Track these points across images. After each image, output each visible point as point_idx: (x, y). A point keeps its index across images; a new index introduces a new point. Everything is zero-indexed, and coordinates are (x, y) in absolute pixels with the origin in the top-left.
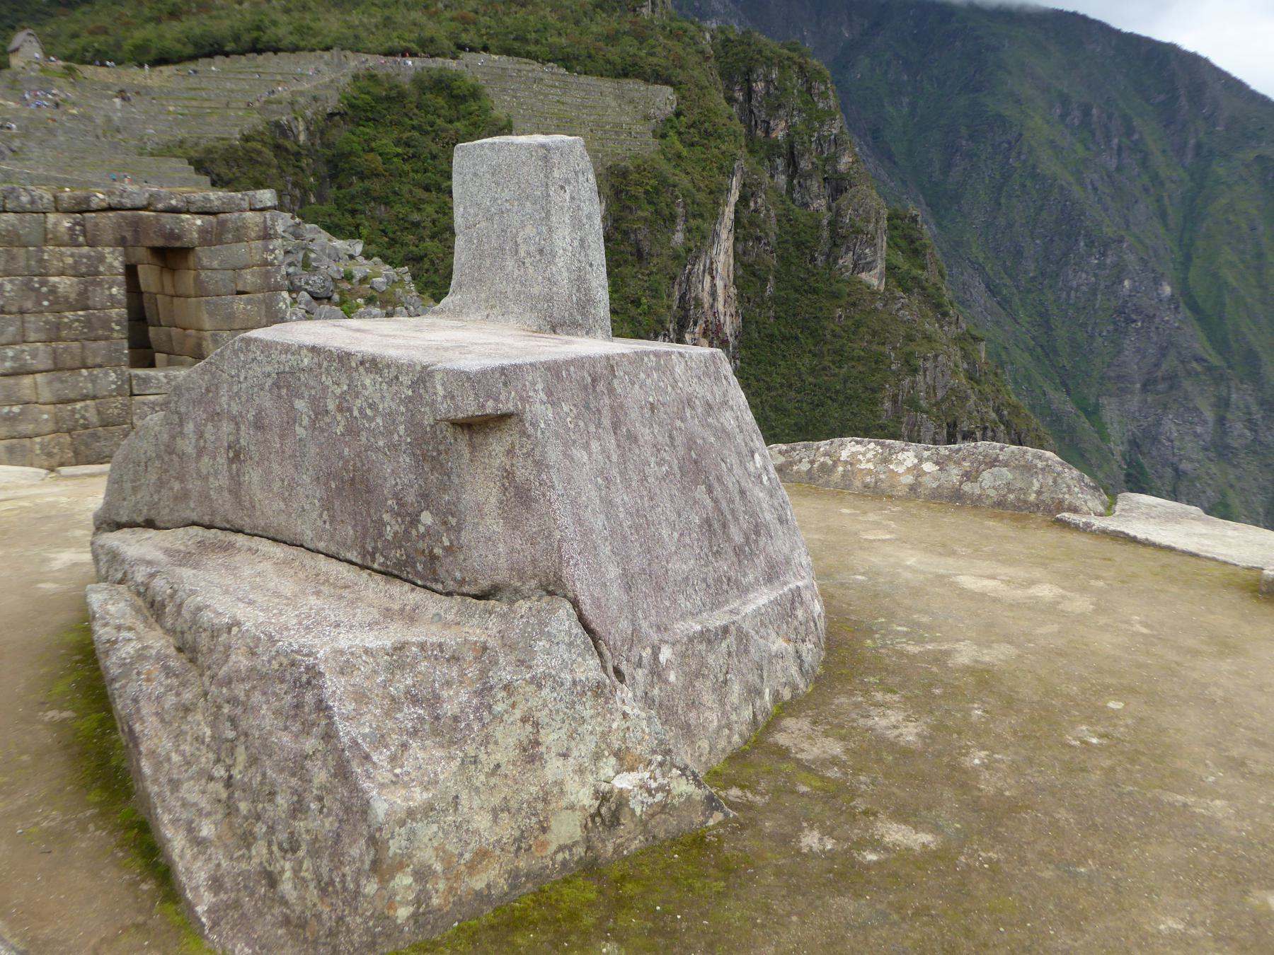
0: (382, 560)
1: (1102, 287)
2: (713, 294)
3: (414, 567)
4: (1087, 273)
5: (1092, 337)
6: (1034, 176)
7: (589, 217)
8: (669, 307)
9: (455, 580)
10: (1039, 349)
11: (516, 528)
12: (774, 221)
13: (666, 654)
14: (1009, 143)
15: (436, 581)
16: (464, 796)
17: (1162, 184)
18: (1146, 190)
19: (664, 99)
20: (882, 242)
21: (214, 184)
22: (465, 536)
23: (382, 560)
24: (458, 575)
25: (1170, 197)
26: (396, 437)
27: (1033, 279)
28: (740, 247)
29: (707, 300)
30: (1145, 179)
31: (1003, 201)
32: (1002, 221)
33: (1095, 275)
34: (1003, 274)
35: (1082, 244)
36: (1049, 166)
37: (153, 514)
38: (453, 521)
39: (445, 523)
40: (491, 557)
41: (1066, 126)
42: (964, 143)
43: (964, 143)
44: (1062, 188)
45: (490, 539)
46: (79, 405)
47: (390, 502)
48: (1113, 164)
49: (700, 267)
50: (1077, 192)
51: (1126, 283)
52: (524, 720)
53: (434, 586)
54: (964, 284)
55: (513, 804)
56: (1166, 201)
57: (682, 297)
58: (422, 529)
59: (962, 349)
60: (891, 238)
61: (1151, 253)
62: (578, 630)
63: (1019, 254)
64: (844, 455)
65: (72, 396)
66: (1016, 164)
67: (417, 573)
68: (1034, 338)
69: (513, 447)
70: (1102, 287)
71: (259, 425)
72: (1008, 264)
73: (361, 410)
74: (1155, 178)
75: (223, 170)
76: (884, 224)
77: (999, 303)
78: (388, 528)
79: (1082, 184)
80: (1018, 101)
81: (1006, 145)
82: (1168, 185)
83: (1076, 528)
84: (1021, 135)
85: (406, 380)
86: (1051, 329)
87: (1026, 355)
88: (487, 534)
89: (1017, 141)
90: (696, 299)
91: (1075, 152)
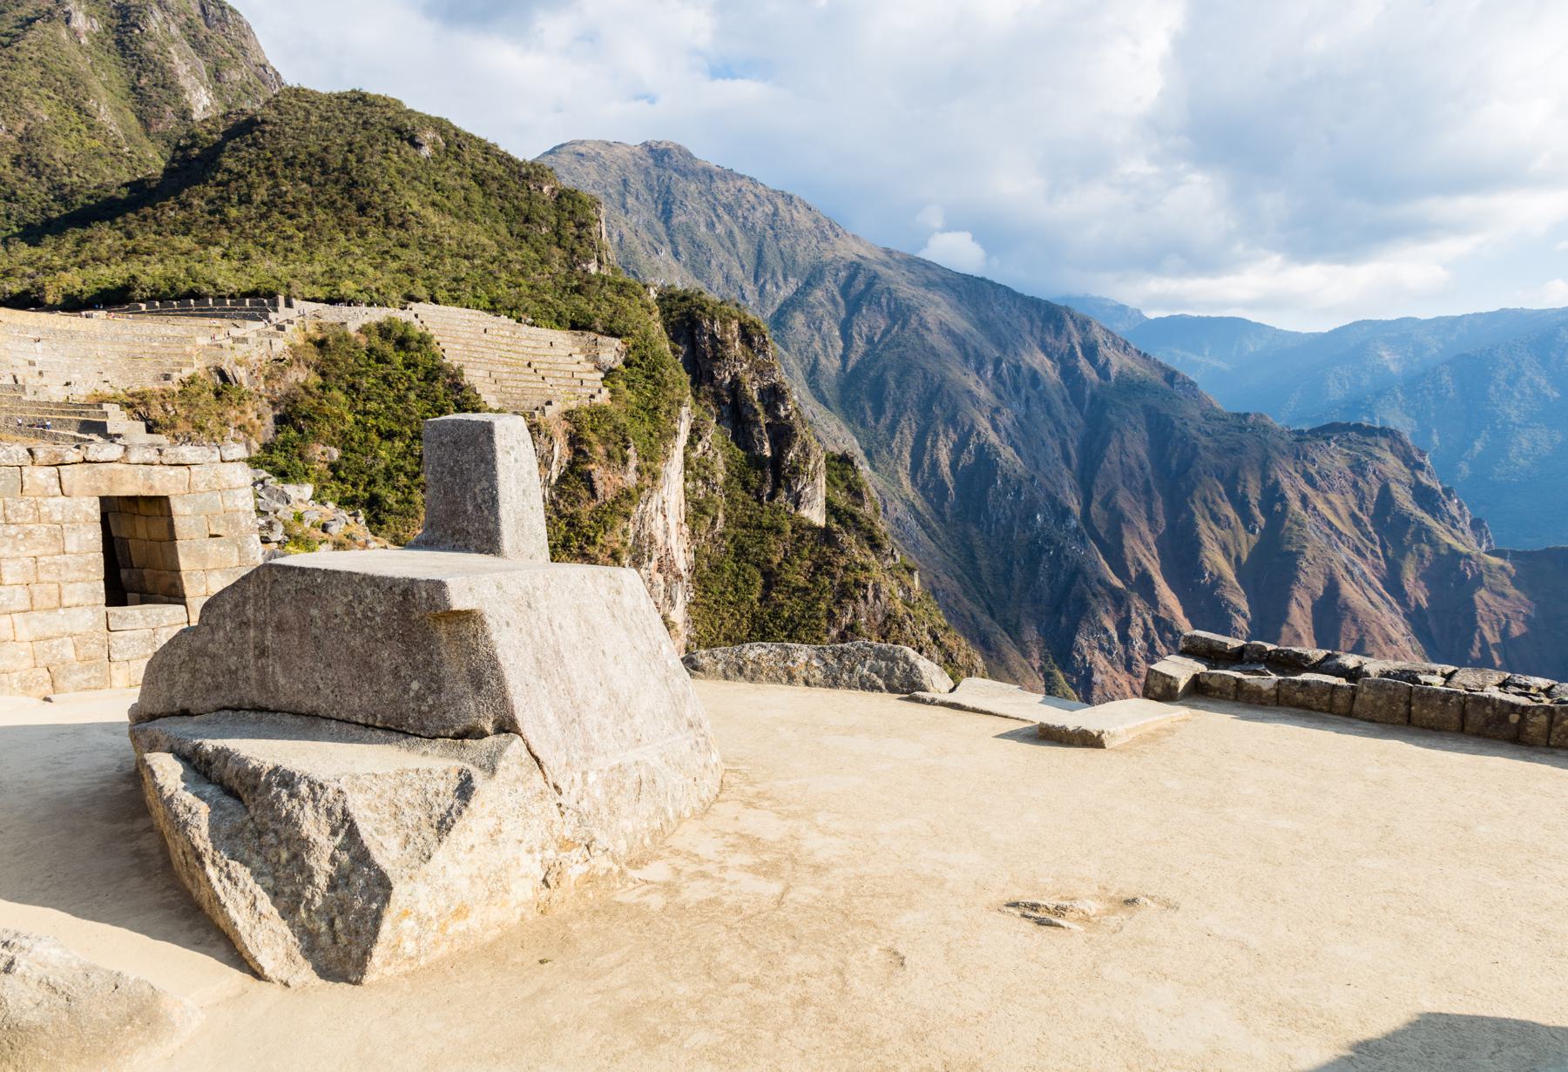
2: (666, 532)
7: (529, 473)
8: (625, 544)
12: (721, 463)
13: (592, 777)
16: (449, 868)
19: (611, 351)
20: (821, 480)
21: (149, 430)
28: (689, 485)
29: (659, 536)
37: (187, 704)
38: (434, 686)
46: (55, 642)
49: (652, 506)
52: (491, 814)
55: (485, 875)
57: (637, 536)
60: (829, 478)
62: (526, 755)
64: (752, 655)
65: (49, 634)
71: (280, 628)
74: (1058, 423)
75: (157, 413)
76: (822, 463)
83: (924, 701)
85: (397, 590)
87: (955, 582)
90: (650, 535)
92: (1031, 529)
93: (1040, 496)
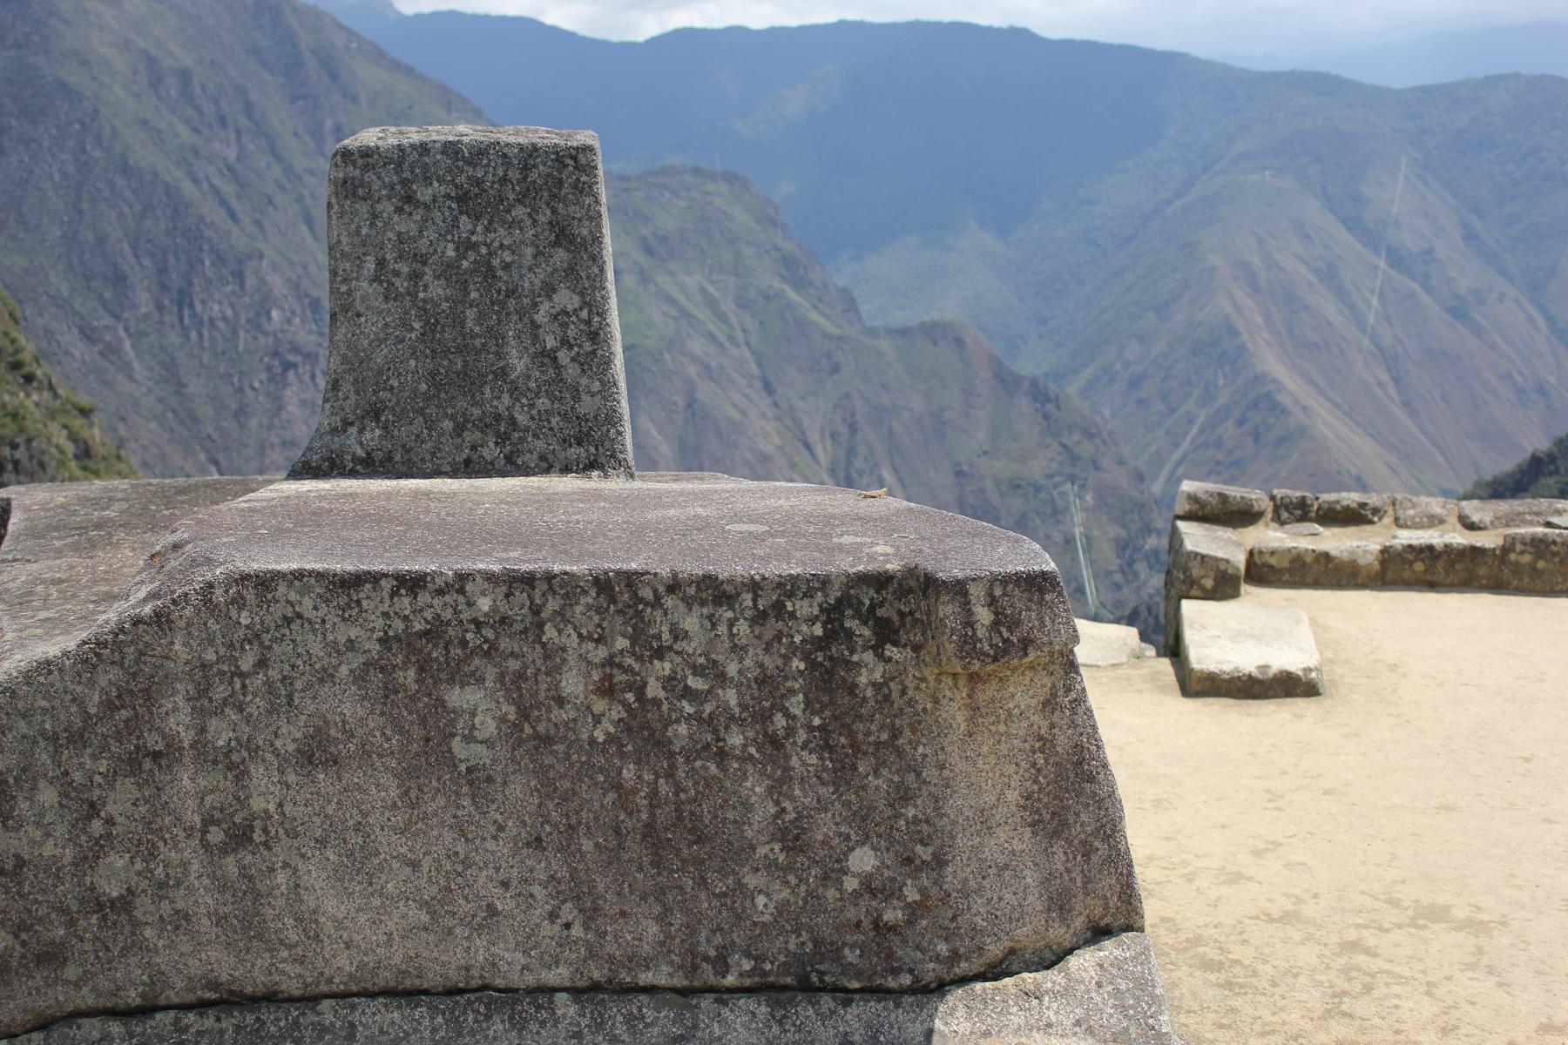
0: (747, 965)
1: (243, 320)
3: (837, 957)
4: (220, 303)
5: (241, 390)
6: (126, 169)
9: (937, 958)
10: (170, 415)
11: (1056, 834)
14: (82, 124)
15: (895, 972)
17: (299, 178)
18: (282, 188)
22: (952, 876)
23: (747, 965)
24: (943, 948)
25: (312, 195)
26: (780, 721)
27: (145, 317)
30: (277, 171)
31: (85, 206)
32: (89, 236)
33: (232, 306)
34: (101, 311)
35: (207, 263)
36: (145, 155)
39: (909, 861)
40: (1008, 897)
41: (161, 99)
42: (13, 123)
43: (13, 123)
44: (167, 186)
45: (1006, 866)
47: (762, 851)
48: (232, 154)
50: (188, 188)
51: (274, 314)
53: (891, 983)
54: (46, 330)
56: (308, 201)
58: (851, 884)
59: (65, 426)
61: (300, 270)
63: (119, 280)
66: (97, 154)
67: (847, 969)
68: (160, 400)
69: (1054, 696)
70: (243, 320)
72: (107, 295)
73: (669, 682)
74: (289, 171)
77: (102, 354)
78: (761, 900)
79: (196, 181)
80: (84, 63)
81: (77, 126)
82: (308, 179)
84: (96, 111)
86: (185, 386)
87: (153, 425)
88: (1001, 860)
89: (93, 120)
91: (177, 135)
92: (266, 334)
93: (277, 282)
